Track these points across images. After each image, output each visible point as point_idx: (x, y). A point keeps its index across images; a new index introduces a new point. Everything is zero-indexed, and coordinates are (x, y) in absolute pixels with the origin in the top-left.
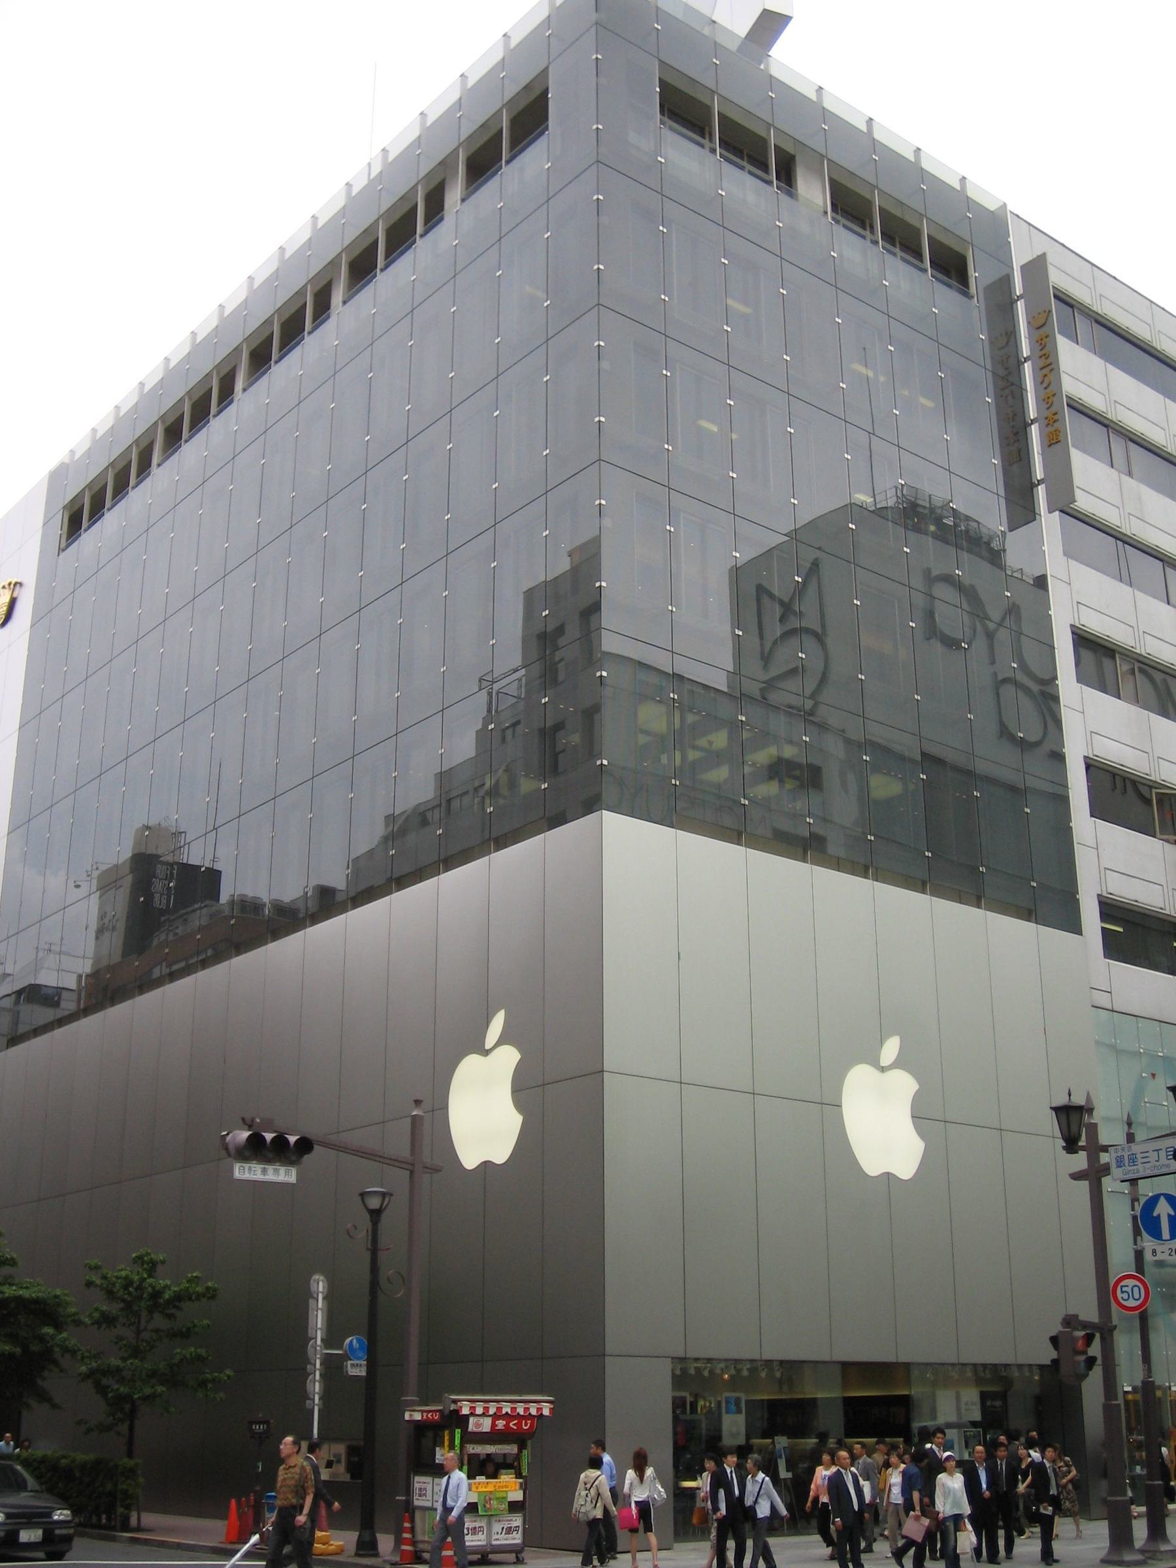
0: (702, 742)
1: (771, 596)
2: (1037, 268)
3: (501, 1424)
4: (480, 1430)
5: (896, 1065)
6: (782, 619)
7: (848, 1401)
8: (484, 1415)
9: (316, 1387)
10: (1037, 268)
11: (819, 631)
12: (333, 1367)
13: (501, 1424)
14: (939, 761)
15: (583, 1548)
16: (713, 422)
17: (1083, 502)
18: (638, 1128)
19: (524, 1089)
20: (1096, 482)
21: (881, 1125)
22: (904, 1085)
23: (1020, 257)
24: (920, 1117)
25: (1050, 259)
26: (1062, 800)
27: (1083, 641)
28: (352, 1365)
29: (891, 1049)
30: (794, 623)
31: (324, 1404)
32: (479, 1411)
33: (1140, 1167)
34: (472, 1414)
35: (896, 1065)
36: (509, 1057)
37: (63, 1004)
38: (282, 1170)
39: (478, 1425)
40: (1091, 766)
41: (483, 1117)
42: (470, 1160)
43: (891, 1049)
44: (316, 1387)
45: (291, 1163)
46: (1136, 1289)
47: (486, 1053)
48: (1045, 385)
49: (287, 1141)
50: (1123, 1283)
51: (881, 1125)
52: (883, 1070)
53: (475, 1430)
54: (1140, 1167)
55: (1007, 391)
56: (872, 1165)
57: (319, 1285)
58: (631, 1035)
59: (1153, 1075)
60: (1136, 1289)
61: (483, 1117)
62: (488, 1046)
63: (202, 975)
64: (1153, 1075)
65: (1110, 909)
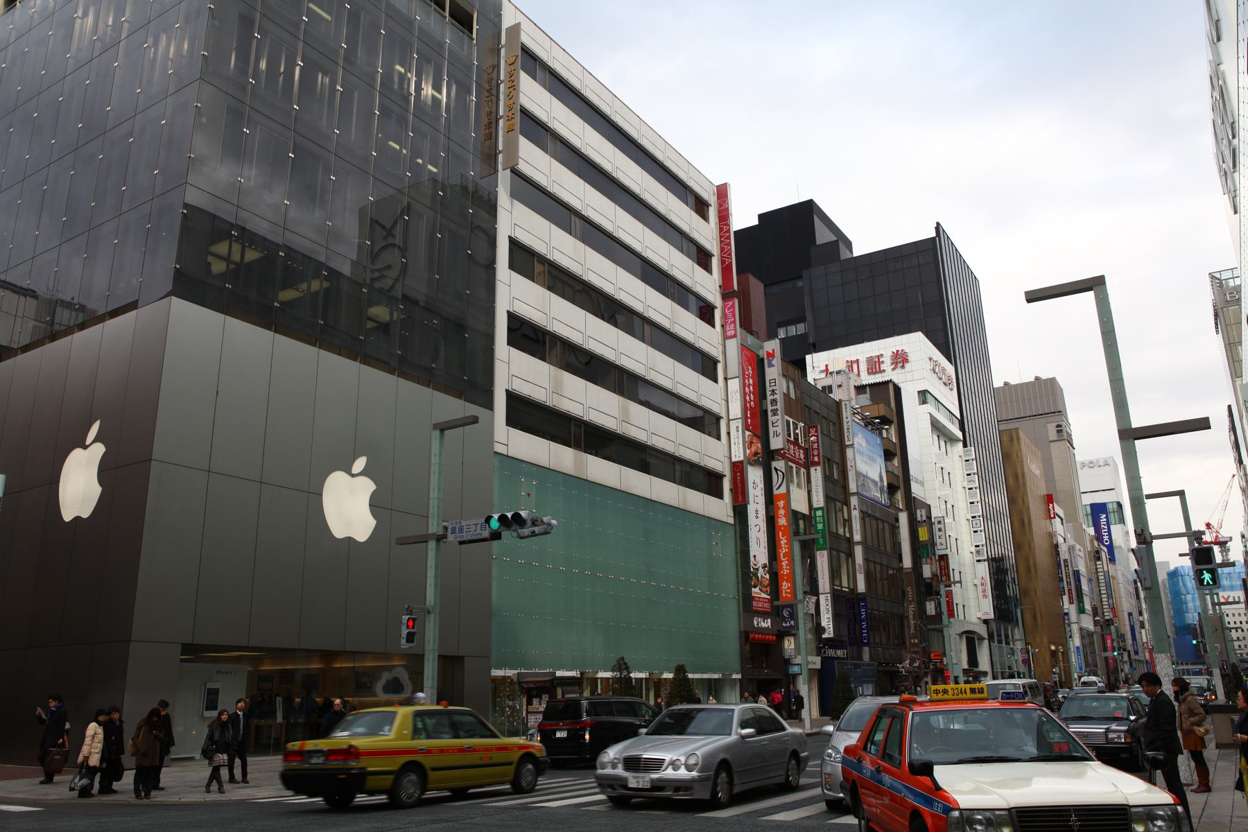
0: (304, 286)
2: (515, 30)
6: (385, 238)
10: (515, 30)
14: (415, 302)
15: (1156, 543)
16: (430, 171)
17: (523, 167)
18: (166, 497)
19: (106, 472)
20: (535, 161)
21: (348, 507)
22: (366, 487)
23: (507, 22)
24: (375, 505)
25: (522, 27)
26: (491, 338)
27: (514, 243)
29: (360, 464)
30: (390, 240)
36: (99, 450)
40: (512, 317)
41: (79, 486)
42: (67, 516)
43: (360, 464)
47: (85, 447)
51: (348, 507)
52: (353, 476)
56: (339, 530)
58: (166, 443)
61: (79, 486)
62: (88, 443)
65: (512, 397)
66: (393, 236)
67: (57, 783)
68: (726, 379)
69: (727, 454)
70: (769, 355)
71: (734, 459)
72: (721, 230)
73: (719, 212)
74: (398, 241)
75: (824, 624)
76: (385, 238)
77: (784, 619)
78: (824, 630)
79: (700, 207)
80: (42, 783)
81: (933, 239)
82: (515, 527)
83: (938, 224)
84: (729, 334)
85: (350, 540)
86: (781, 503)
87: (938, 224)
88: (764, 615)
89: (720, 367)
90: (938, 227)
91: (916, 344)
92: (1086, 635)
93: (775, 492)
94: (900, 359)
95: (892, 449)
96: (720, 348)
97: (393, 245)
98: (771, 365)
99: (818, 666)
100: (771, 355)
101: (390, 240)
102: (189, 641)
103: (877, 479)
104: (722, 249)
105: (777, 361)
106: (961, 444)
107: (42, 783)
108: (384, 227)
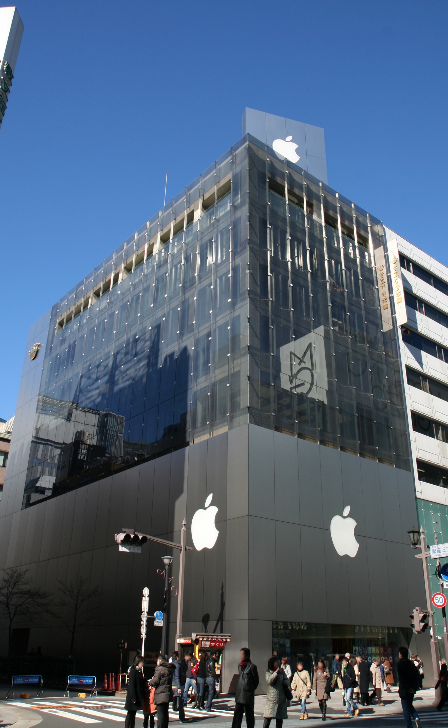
1: (295, 355)
3: (213, 644)
4: (206, 646)
5: (348, 516)
6: (299, 364)
7: (334, 640)
8: (207, 640)
9: (143, 630)
11: (311, 368)
12: (150, 622)
13: (213, 644)
19: (220, 522)
21: (344, 536)
22: (351, 523)
24: (358, 534)
28: (157, 622)
29: (347, 511)
30: (303, 365)
31: (146, 636)
32: (205, 639)
33: (442, 553)
34: (203, 640)
35: (348, 516)
36: (214, 510)
37: (46, 494)
38: (136, 548)
39: (205, 645)
43: (347, 511)
44: (143, 630)
45: (140, 546)
46: (441, 599)
47: (205, 509)
48: (396, 282)
49: (139, 537)
50: (436, 596)
52: (344, 518)
53: (204, 646)
54: (442, 553)
55: (383, 285)
57: (146, 591)
59: (437, 523)
60: (441, 599)
62: (206, 506)
63: (102, 481)
64: (437, 523)
65: (421, 463)
66: (305, 363)
74: (309, 365)
76: (299, 364)
85: (346, 556)
88: (346, 658)
92: (272, 301)
97: (305, 368)
101: (303, 365)
108: (298, 358)
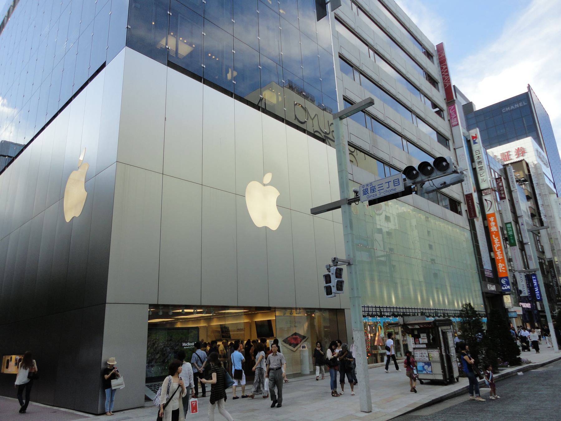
22: (273, 194)
29: (268, 178)
43: (268, 178)
52: (264, 185)
56: (258, 220)
67: (28, 413)
68: (455, 149)
69: (461, 190)
70: (473, 137)
71: (466, 193)
72: (442, 68)
73: (440, 59)
75: (520, 288)
77: (502, 285)
78: (521, 292)
79: (429, 55)
80: (225, 401)
81: (527, 93)
82: (436, 173)
83: (529, 85)
84: (454, 124)
86: (492, 219)
87: (529, 85)
89: (451, 142)
90: (529, 87)
91: (527, 143)
93: (487, 213)
94: (521, 151)
95: (530, 195)
96: (450, 132)
98: (475, 143)
99: (521, 313)
100: (475, 138)
102: (339, 8)
103: (526, 211)
104: (444, 79)
105: (479, 140)
106: (556, 195)
107: (225, 401)
